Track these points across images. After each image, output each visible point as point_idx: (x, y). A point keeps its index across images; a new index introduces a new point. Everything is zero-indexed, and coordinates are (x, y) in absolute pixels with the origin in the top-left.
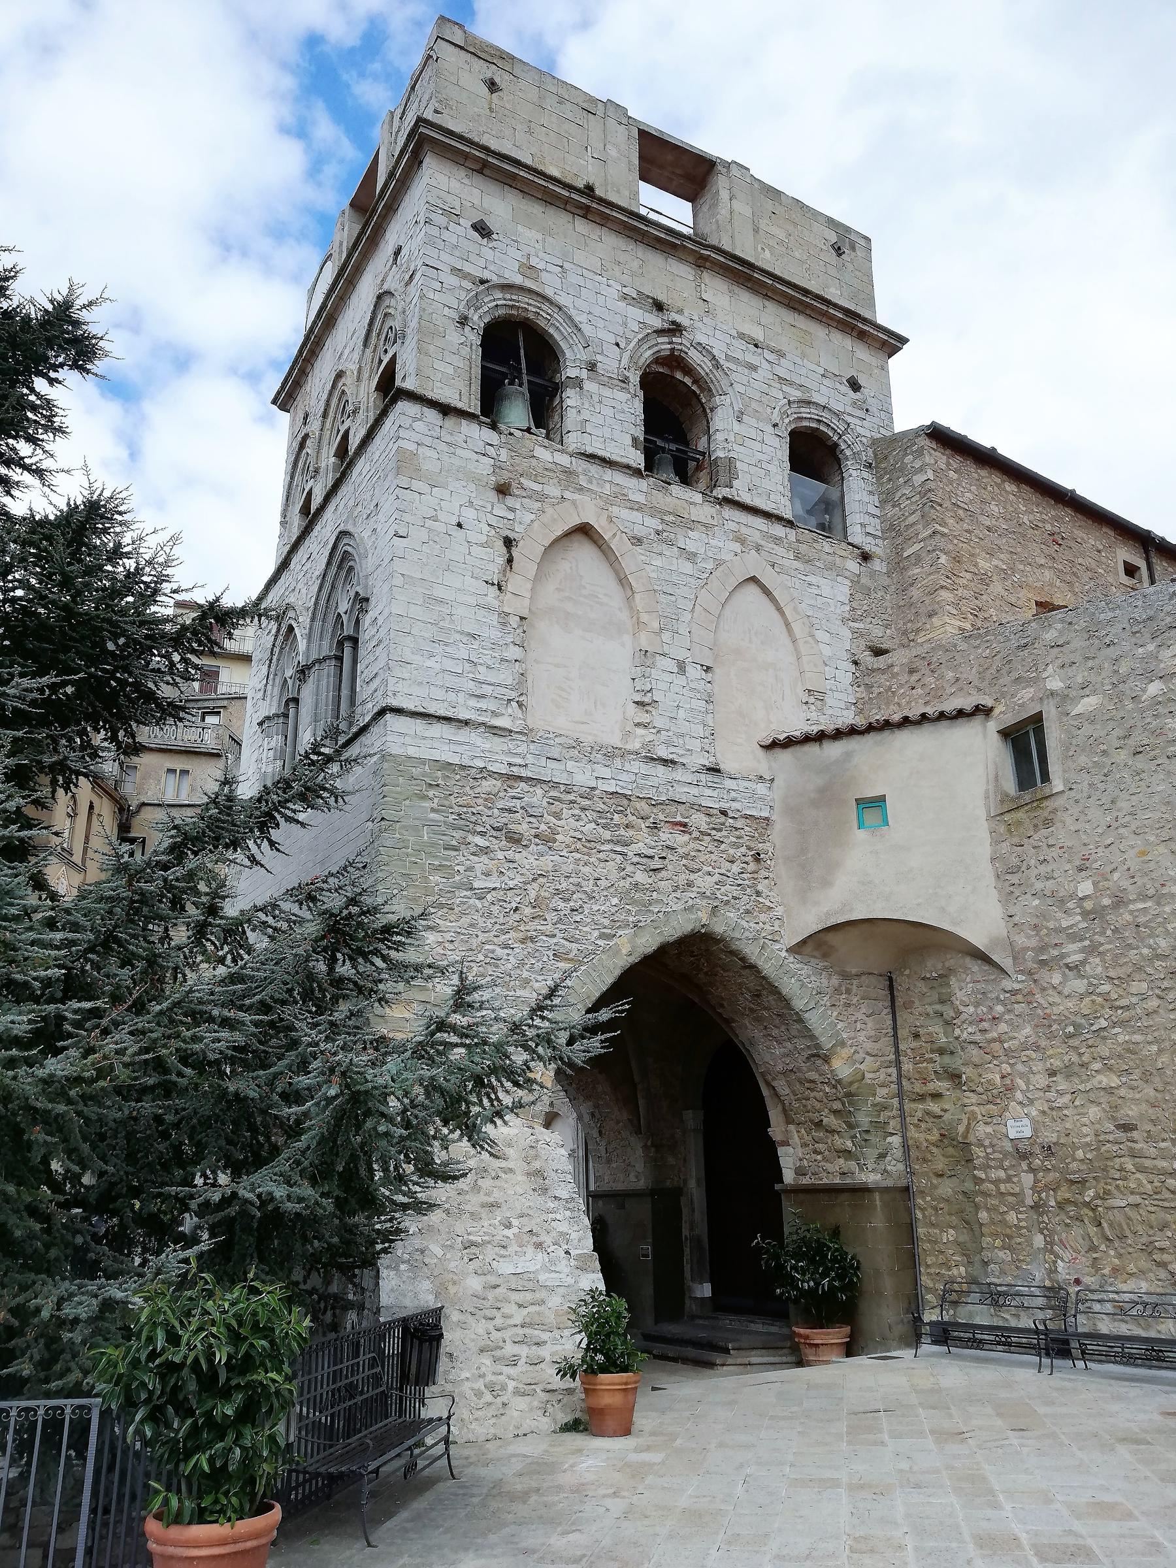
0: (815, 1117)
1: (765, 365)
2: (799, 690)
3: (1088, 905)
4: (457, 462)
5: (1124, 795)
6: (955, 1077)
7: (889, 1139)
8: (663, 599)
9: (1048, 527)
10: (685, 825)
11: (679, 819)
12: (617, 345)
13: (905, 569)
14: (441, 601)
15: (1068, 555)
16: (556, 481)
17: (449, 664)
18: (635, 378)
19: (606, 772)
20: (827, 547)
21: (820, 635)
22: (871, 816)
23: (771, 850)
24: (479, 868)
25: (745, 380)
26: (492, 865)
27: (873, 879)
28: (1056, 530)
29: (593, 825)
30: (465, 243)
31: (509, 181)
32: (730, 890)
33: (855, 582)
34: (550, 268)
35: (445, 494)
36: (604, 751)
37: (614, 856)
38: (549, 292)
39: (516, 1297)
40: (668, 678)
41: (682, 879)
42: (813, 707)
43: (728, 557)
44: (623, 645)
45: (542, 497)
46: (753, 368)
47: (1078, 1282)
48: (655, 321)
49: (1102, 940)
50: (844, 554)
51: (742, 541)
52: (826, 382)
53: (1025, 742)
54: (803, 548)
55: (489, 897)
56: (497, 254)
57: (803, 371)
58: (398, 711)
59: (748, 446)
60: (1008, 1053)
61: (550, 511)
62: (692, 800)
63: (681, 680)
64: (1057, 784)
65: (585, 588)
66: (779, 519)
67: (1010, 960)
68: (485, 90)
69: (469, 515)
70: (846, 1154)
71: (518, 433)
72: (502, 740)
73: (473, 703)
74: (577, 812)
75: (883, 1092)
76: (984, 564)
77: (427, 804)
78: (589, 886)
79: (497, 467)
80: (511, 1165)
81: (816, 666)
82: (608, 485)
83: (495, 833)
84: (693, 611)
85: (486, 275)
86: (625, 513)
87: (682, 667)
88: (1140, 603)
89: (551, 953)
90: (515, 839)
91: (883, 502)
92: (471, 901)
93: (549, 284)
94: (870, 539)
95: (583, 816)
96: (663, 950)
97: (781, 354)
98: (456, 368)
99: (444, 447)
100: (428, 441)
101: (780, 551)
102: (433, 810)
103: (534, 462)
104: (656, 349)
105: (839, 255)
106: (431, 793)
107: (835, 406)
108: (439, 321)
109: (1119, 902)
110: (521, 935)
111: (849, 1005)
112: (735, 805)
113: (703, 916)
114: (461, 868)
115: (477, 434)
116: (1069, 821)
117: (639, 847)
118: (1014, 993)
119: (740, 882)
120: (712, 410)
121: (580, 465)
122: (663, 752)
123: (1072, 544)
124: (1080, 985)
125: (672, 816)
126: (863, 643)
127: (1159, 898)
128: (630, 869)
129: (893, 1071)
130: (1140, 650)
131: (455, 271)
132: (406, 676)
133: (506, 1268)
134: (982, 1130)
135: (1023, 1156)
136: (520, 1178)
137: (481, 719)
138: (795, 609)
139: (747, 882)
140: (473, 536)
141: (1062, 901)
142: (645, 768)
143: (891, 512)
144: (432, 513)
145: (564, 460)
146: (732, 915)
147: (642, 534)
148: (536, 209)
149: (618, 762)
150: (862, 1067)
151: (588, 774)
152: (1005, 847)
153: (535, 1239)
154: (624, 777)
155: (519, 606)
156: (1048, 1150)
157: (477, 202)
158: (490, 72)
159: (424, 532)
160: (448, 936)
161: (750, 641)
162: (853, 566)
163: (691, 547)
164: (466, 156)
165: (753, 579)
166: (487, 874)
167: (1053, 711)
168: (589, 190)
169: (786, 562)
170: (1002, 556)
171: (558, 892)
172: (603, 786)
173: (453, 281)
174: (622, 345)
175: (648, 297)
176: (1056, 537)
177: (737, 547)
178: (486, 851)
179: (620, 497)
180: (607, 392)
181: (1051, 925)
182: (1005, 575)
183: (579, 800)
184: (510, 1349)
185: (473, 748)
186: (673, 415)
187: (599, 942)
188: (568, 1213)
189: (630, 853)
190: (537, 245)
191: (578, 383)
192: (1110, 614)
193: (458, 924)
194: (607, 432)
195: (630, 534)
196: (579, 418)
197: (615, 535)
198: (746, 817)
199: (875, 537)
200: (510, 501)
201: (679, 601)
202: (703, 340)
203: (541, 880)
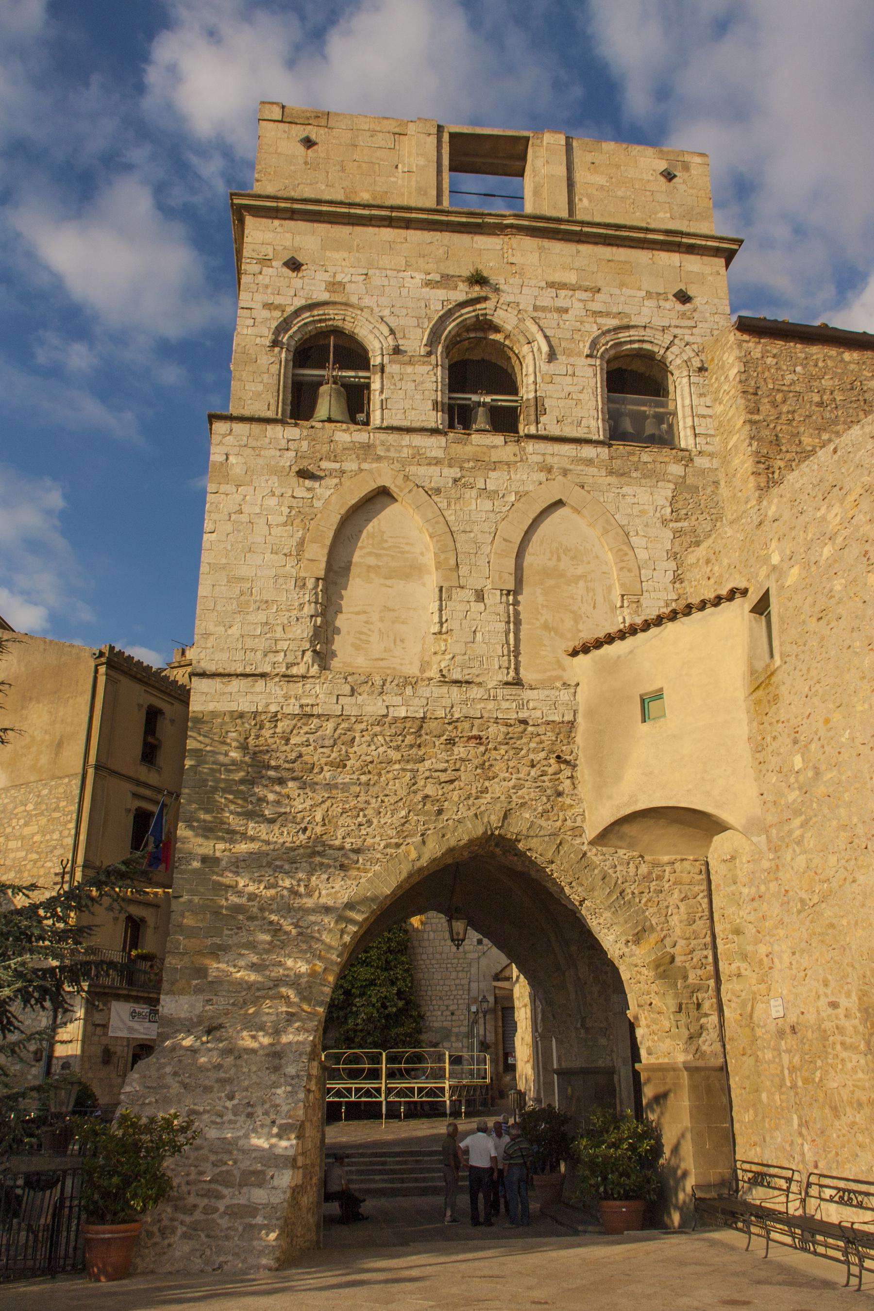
10: (480, 738)
14: (242, 579)
19: (398, 700)
31: (317, 218)
39: (213, 1158)
40: (464, 607)
50: (666, 459)
53: (762, 607)
54: (617, 464)
65: (386, 541)
68: (301, 149)
82: (405, 450)
84: (492, 542)
86: (422, 470)
87: (480, 596)
101: (592, 470)
113: (495, 819)
121: (382, 436)
122: (456, 676)
131: (268, 306)
139: (547, 783)
144: (237, 508)
151: (380, 703)
158: (301, 132)
173: (266, 313)
177: (542, 476)
179: (419, 458)
180: (409, 369)
198: (548, 723)
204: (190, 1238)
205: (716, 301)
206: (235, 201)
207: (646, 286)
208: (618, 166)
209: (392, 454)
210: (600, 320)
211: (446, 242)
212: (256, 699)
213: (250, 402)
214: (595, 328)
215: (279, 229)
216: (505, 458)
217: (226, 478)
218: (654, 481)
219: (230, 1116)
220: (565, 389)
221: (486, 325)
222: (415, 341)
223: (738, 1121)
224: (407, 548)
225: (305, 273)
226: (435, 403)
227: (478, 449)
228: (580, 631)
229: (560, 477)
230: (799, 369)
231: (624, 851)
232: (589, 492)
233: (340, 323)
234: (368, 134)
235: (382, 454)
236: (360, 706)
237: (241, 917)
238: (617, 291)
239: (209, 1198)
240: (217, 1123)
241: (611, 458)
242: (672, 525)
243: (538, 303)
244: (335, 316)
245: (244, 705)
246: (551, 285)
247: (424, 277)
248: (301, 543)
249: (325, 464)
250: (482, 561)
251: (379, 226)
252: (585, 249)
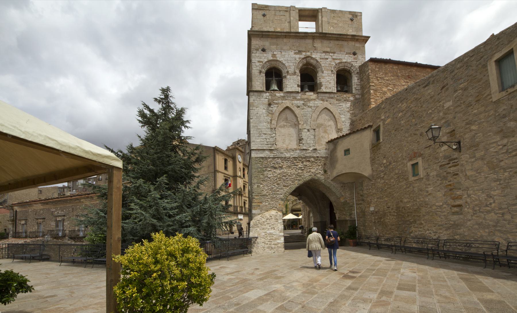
1: (330, 57)
6: (363, 200)
17: (262, 140)
18: (298, 72)
19: (292, 153)
27: (343, 166)
46: (327, 59)
53: (377, 132)
60: (371, 195)
64: (381, 140)
68: (262, 17)
70: (345, 215)
91: (361, 81)
109: (390, 163)
117: (300, 166)
124: (383, 181)
125: (307, 159)
131: (259, 62)
133: (268, 232)
134: (367, 209)
135: (372, 214)
141: (381, 165)
143: (362, 83)
148: (274, 41)
152: (372, 155)
155: (273, 126)
156: (376, 212)
163: (311, 105)
164: (259, 35)
165: (326, 108)
178: (270, 171)
184: (267, 243)
185: (266, 154)
186: (309, 79)
207: (346, 51)
220: (328, 80)
246: (324, 52)
248: (271, 120)
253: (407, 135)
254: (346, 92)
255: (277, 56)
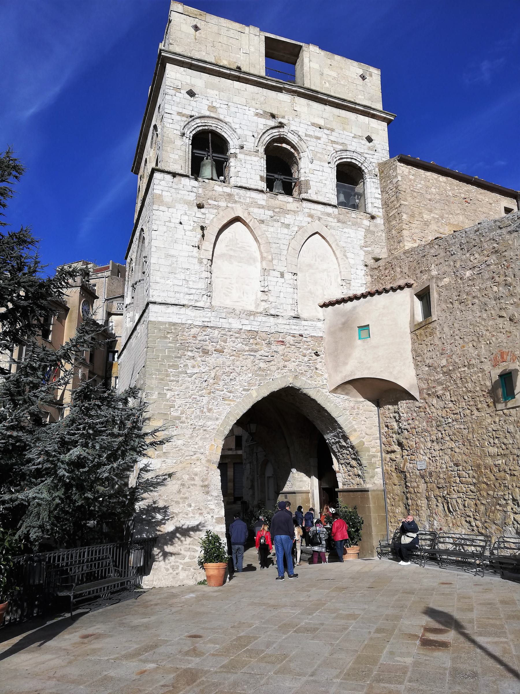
0: (348, 461)
1: (325, 136)
2: (339, 279)
3: (445, 369)
4: (179, 196)
5: (457, 321)
7: (376, 470)
8: (274, 246)
9: (463, 196)
11: (280, 339)
12: (253, 136)
13: (390, 221)
15: (473, 207)
16: (224, 199)
17: (177, 282)
18: (262, 149)
19: (247, 322)
20: (353, 215)
21: (349, 255)
22: (364, 333)
23: (323, 350)
24: (190, 365)
25: (314, 144)
26: (195, 363)
28: (467, 196)
29: (241, 344)
30: (183, 101)
32: (303, 368)
33: (368, 231)
34: (222, 106)
35: (175, 210)
36: (246, 313)
37: (250, 357)
38: (221, 117)
40: (275, 279)
41: (281, 365)
42: (345, 287)
43: (304, 224)
44: (256, 267)
45: (218, 207)
46: (318, 138)
47: (441, 529)
48: (272, 123)
49: (449, 384)
50: (362, 217)
51: (311, 216)
52: (355, 140)
54: (341, 217)
55: (194, 376)
56: (198, 103)
57: (344, 136)
58: (154, 303)
59: (317, 175)
61: (221, 213)
62: (285, 331)
63: (282, 280)
66: (330, 205)
67: (418, 394)
68: (193, 31)
69: (184, 219)
71: (207, 181)
72: (200, 311)
73: (187, 297)
74: (233, 339)
75: (374, 450)
76: (426, 216)
77: (168, 340)
78: (238, 370)
79: (198, 196)
80: (196, 483)
81: (346, 268)
82: (248, 199)
83: (197, 350)
85: (193, 113)
86: (256, 210)
87: (282, 275)
88: (464, 236)
89: (221, 398)
90: (206, 352)
92: (186, 378)
93: (222, 113)
94: (376, 209)
95: (236, 341)
96: (273, 395)
97: (332, 130)
98: (179, 156)
99: (173, 190)
100: (166, 189)
102: (170, 342)
103: (214, 192)
104: (271, 136)
105: (364, 80)
106: (169, 336)
107: (359, 150)
108: (171, 136)
110: (208, 391)
111: (358, 414)
112: (306, 332)
114: (182, 366)
115: (189, 183)
116: (438, 333)
117: (262, 352)
118: (420, 407)
119: (308, 364)
120: (300, 159)
121: (237, 190)
122: (273, 312)
123: (477, 202)
124: (442, 404)
126: (370, 256)
127: (469, 366)
128: (257, 361)
129: (378, 441)
130: (464, 256)
131: (179, 114)
132: (158, 288)
136: (199, 488)
137: (190, 304)
138: (337, 245)
140: (187, 227)
142: (264, 319)
144: (168, 219)
145: (228, 190)
146: (304, 379)
147: (264, 219)
149: (252, 318)
150: (364, 440)
153: (200, 511)
154: (255, 323)
157: (189, 82)
159: (165, 228)
160: (176, 393)
161: (316, 261)
162: (366, 222)
163: (287, 222)
166: (193, 367)
167: (434, 285)
168: (239, 69)
169: (333, 224)
170: (436, 212)
171: (224, 373)
172: (244, 328)
173: (179, 118)
174: (256, 136)
175: (268, 112)
176: (467, 200)
177: (309, 219)
178: (193, 358)
180: (248, 158)
181: (432, 378)
182: (437, 221)
183: (234, 334)
186: (281, 166)
187: (243, 392)
188: (216, 501)
189: (258, 355)
190: (216, 97)
191: (235, 155)
192: (454, 241)
193: (181, 388)
194: (248, 176)
195: (259, 219)
196: (236, 170)
197: (251, 220)
199: (378, 208)
200: (202, 210)
201: (282, 245)
202: (293, 128)
203: (217, 368)
204: (185, 570)
205: (383, 143)
206: (163, 54)
208: (341, 69)
209: (241, 200)
210: (334, 145)
211: (265, 94)
212: (181, 317)
213: (172, 164)
214: (332, 149)
215: (184, 73)
216: (293, 209)
217: (162, 203)
218: (357, 227)
219: (191, 515)
221: (282, 140)
222: (250, 144)
223: (222, 507)
224: (248, 248)
225: (197, 99)
226: (261, 177)
227: (281, 202)
228: (325, 295)
229: (317, 221)
230: (422, 182)
231: (343, 396)
232: (329, 229)
233: (214, 129)
234: (226, 29)
235: (237, 200)
236: (230, 323)
237: (177, 421)
238: (341, 132)
239: (190, 551)
240: (185, 518)
241: (339, 214)
242: (365, 249)
243: (307, 133)
244: (212, 125)
245: (175, 319)
246: (313, 124)
247: (255, 110)
249: (210, 202)
250: (283, 258)
251: (233, 80)
252: (328, 108)
253: (485, 316)
254: (355, 207)
255: (219, 110)
